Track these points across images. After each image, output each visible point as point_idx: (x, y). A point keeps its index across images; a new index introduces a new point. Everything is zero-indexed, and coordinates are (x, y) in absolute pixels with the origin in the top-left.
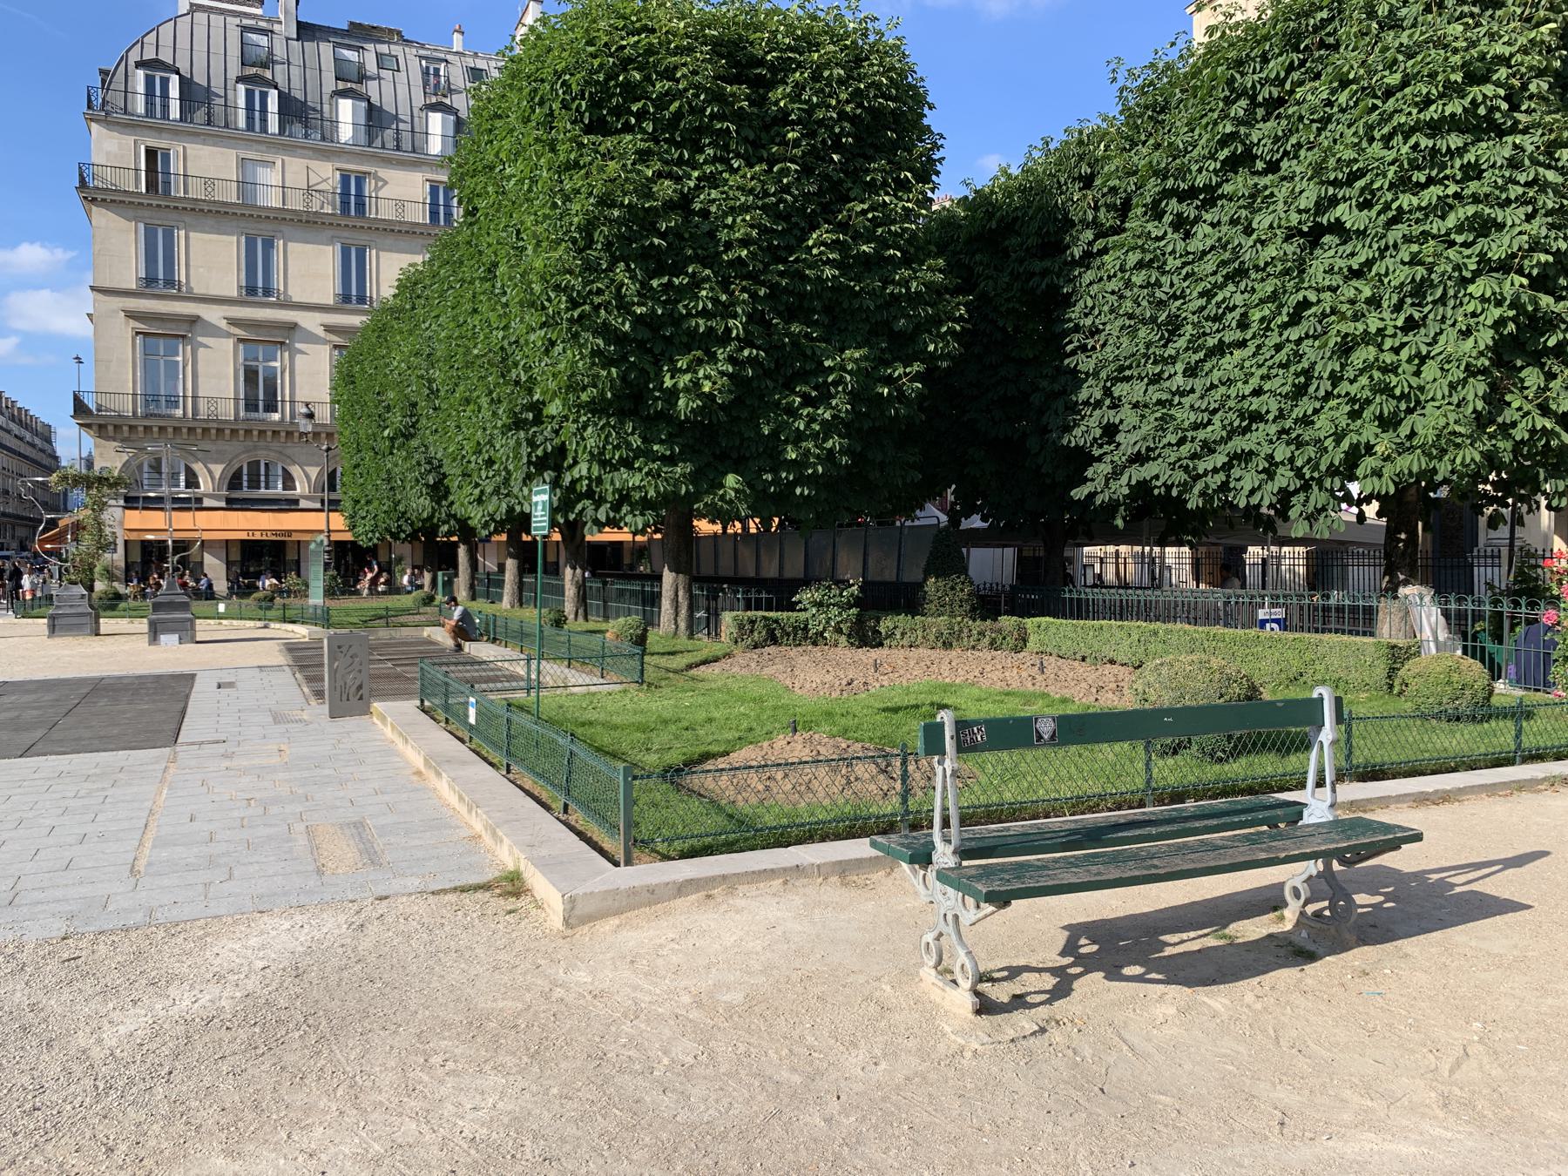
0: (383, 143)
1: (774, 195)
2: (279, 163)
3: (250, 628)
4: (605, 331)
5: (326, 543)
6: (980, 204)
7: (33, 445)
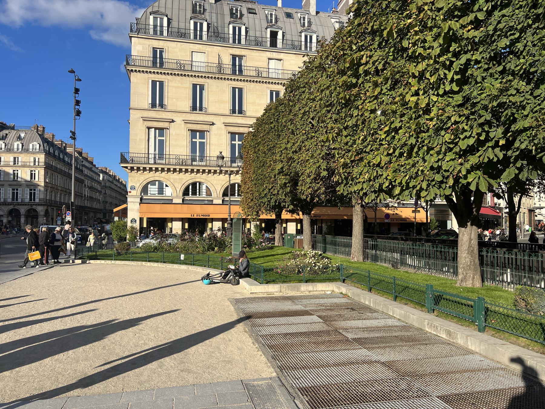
7: (120, 188)
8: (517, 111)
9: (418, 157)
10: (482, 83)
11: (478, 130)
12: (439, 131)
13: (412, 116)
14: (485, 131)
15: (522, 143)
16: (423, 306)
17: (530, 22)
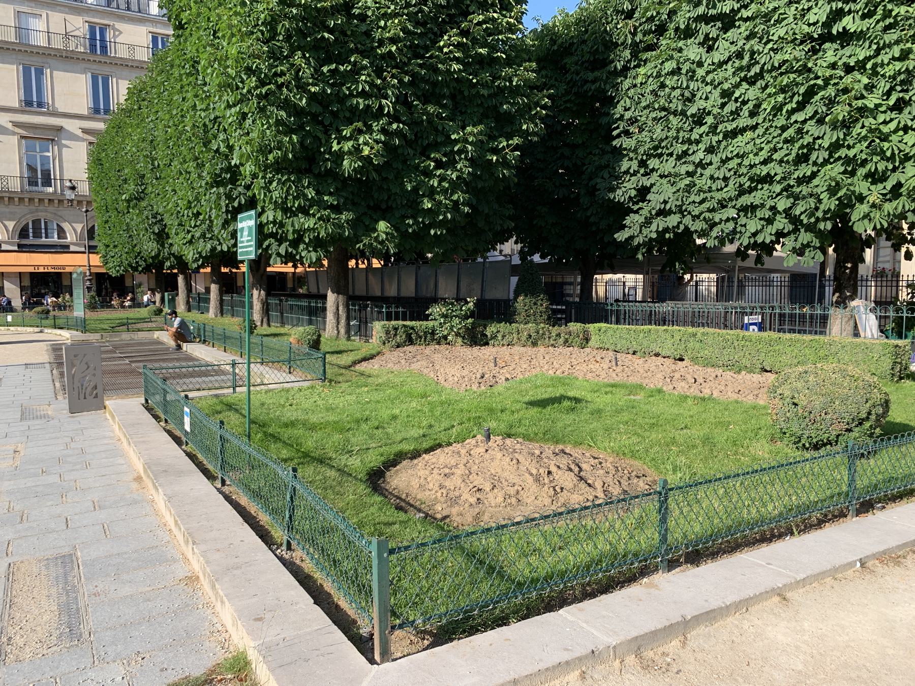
0: (118, 5)
1: (415, 5)
2: (44, 16)
3: (30, 333)
4: (286, 105)
5: (88, 274)
6: (547, 34)
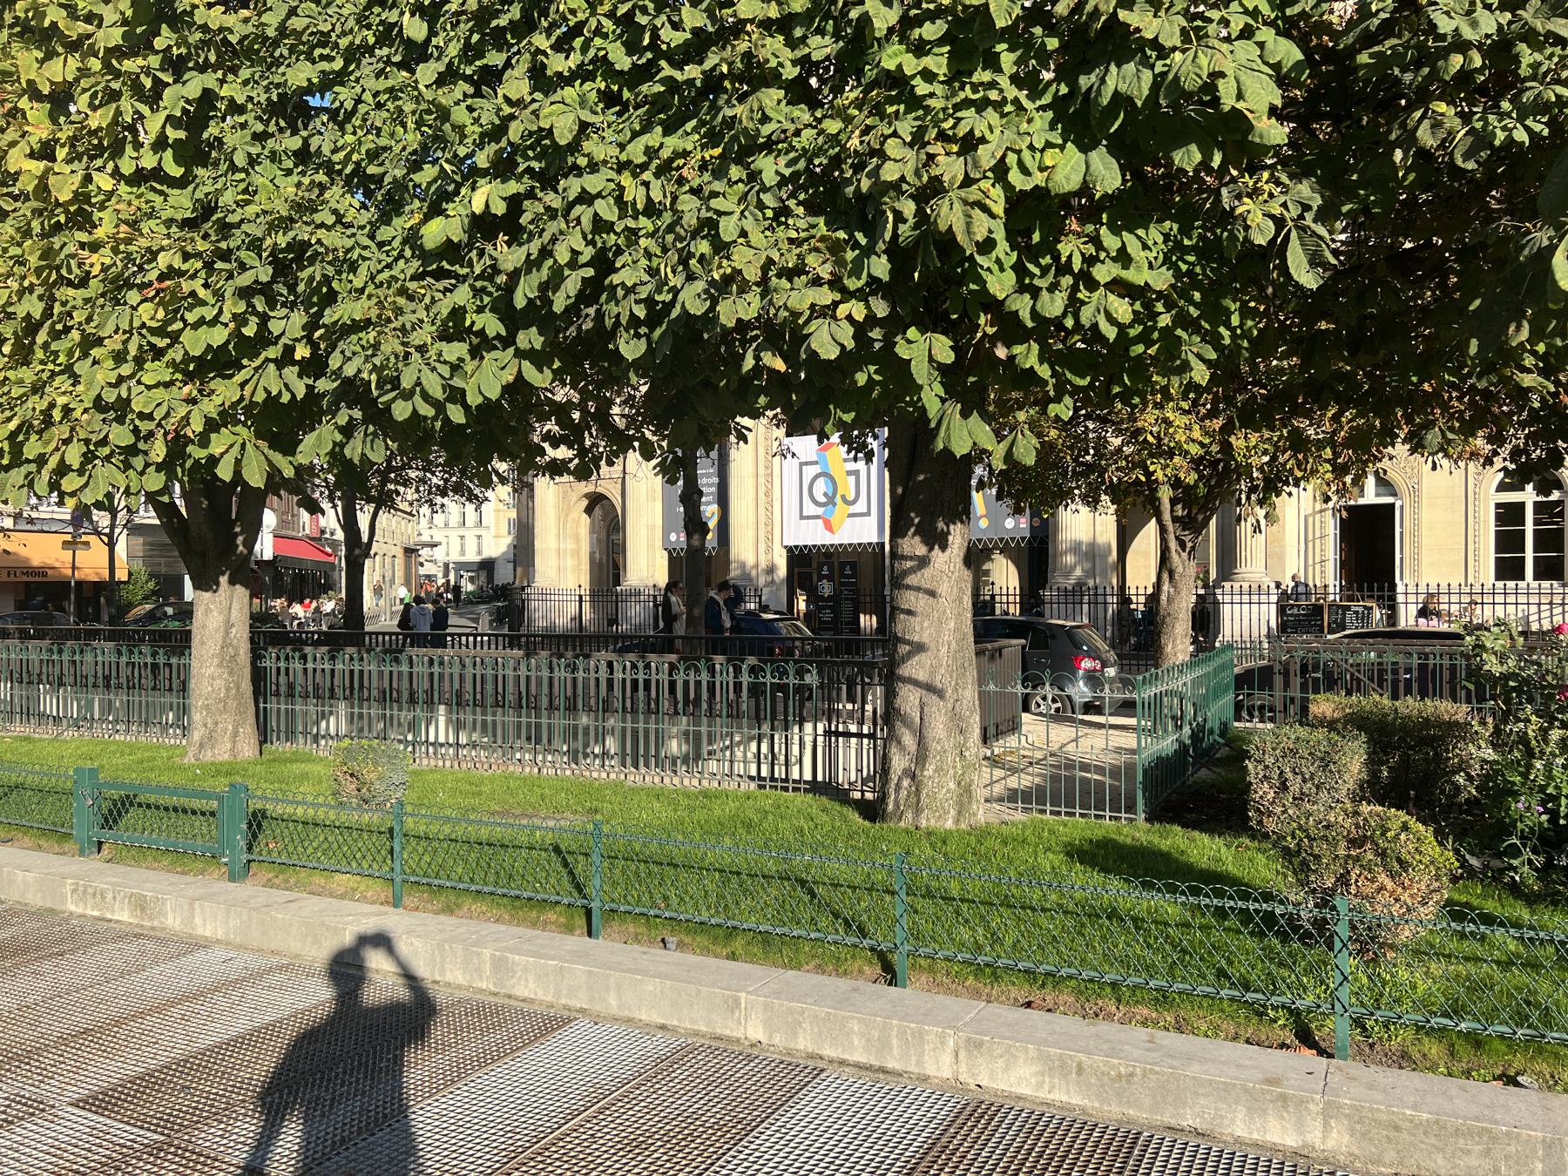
8: (339, 273)
9: (54, 362)
10: (248, 174)
11: (235, 304)
12: (120, 289)
13: (29, 224)
14: (255, 313)
15: (349, 361)
16: (67, 836)
17: (371, 40)
